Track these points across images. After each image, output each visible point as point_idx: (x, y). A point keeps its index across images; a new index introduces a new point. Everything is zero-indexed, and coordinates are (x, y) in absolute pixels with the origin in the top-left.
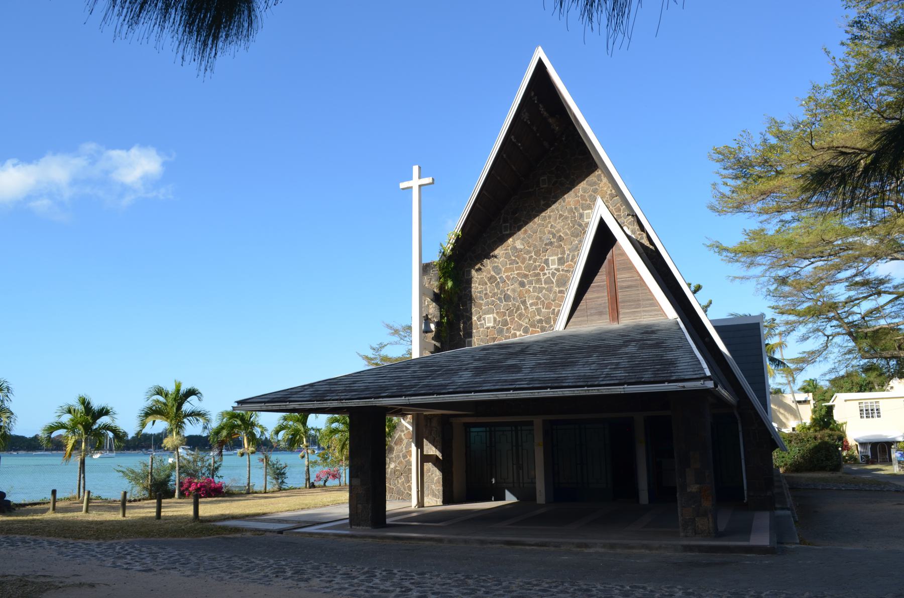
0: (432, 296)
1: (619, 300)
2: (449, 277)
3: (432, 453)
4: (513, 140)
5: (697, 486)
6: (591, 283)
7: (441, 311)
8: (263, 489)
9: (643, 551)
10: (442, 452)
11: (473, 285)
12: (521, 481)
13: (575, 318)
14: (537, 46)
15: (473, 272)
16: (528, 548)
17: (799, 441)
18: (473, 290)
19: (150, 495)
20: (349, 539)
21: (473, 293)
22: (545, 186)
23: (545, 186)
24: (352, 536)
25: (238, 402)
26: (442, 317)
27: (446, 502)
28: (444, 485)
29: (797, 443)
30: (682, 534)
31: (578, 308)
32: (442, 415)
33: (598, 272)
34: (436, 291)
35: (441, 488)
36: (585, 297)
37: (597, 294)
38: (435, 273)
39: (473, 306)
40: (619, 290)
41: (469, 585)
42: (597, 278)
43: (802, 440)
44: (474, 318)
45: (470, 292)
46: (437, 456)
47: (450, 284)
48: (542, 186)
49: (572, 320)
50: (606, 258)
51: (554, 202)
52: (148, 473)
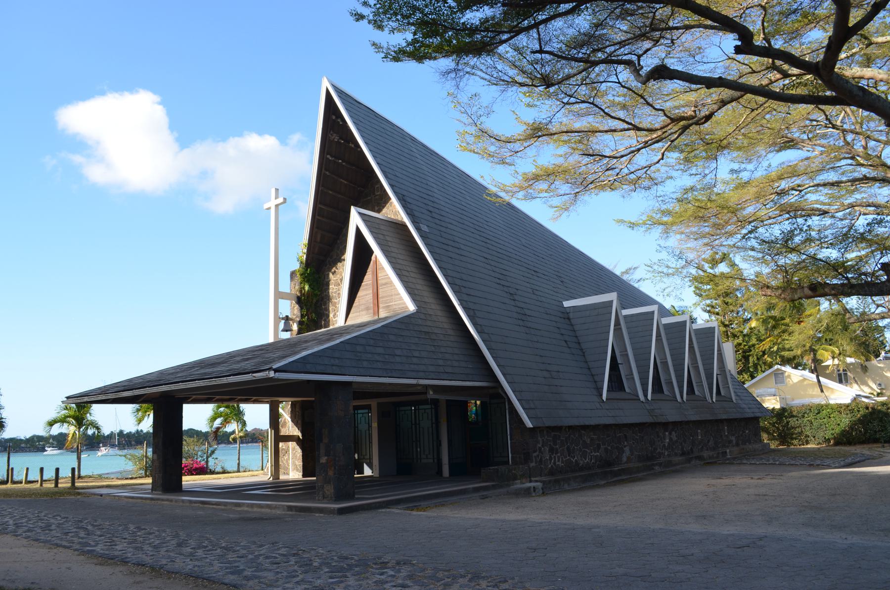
0: (296, 299)
1: (380, 296)
2: (308, 281)
3: (296, 434)
4: (330, 158)
5: (326, 458)
6: (362, 282)
7: (301, 312)
8: (236, 469)
9: (267, 510)
10: (302, 432)
11: (330, 287)
12: (419, 457)
13: (353, 313)
14: (322, 77)
15: (331, 275)
16: (211, 506)
17: (848, 412)
18: (330, 291)
19: (146, 474)
20: (131, 500)
21: (331, 294)
22: (378, 193)
23: (378, 193)
24: (152, 499)
25: (68, 398)
26: (302, 316)
27: (304, 476)
28: (303, 461)
29: (847, 414)
30: (317, 498)
31: (354, 305)
32: (302, 401)
33: (366, 272)
34: (299, 295)
35: (302, 464)
36: (358, 295)
37: (365, 293)
38: (298, 278)
39: (330, 305)
40: (380, 287)
41: (98, 529)
42: (366, 277)
43: (852, 411)
44: (331, 315)
45: (329, 293)
46: (299, 437)
47: (307, 288)
48: (377, 194)
49: (350, 316)
50: (371, 260)
51: (384, 207)
52: (143, 456)
